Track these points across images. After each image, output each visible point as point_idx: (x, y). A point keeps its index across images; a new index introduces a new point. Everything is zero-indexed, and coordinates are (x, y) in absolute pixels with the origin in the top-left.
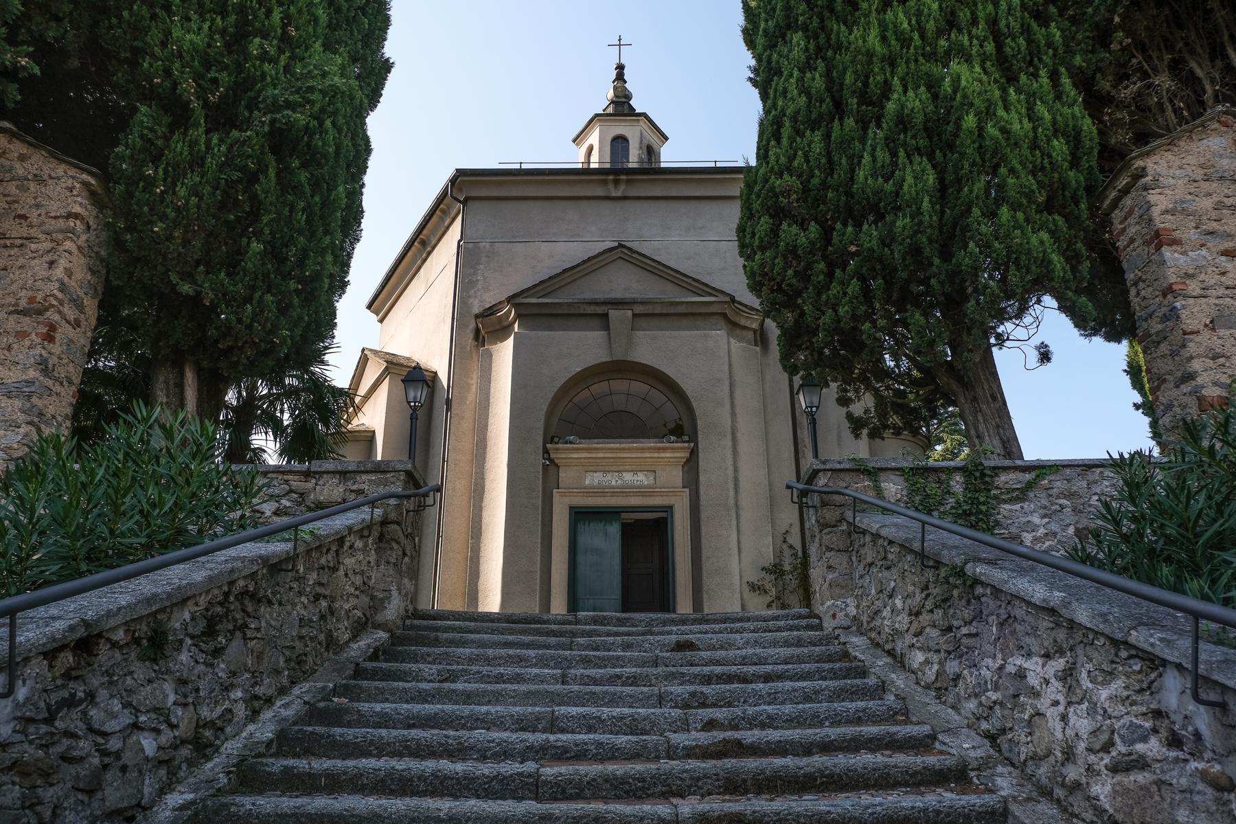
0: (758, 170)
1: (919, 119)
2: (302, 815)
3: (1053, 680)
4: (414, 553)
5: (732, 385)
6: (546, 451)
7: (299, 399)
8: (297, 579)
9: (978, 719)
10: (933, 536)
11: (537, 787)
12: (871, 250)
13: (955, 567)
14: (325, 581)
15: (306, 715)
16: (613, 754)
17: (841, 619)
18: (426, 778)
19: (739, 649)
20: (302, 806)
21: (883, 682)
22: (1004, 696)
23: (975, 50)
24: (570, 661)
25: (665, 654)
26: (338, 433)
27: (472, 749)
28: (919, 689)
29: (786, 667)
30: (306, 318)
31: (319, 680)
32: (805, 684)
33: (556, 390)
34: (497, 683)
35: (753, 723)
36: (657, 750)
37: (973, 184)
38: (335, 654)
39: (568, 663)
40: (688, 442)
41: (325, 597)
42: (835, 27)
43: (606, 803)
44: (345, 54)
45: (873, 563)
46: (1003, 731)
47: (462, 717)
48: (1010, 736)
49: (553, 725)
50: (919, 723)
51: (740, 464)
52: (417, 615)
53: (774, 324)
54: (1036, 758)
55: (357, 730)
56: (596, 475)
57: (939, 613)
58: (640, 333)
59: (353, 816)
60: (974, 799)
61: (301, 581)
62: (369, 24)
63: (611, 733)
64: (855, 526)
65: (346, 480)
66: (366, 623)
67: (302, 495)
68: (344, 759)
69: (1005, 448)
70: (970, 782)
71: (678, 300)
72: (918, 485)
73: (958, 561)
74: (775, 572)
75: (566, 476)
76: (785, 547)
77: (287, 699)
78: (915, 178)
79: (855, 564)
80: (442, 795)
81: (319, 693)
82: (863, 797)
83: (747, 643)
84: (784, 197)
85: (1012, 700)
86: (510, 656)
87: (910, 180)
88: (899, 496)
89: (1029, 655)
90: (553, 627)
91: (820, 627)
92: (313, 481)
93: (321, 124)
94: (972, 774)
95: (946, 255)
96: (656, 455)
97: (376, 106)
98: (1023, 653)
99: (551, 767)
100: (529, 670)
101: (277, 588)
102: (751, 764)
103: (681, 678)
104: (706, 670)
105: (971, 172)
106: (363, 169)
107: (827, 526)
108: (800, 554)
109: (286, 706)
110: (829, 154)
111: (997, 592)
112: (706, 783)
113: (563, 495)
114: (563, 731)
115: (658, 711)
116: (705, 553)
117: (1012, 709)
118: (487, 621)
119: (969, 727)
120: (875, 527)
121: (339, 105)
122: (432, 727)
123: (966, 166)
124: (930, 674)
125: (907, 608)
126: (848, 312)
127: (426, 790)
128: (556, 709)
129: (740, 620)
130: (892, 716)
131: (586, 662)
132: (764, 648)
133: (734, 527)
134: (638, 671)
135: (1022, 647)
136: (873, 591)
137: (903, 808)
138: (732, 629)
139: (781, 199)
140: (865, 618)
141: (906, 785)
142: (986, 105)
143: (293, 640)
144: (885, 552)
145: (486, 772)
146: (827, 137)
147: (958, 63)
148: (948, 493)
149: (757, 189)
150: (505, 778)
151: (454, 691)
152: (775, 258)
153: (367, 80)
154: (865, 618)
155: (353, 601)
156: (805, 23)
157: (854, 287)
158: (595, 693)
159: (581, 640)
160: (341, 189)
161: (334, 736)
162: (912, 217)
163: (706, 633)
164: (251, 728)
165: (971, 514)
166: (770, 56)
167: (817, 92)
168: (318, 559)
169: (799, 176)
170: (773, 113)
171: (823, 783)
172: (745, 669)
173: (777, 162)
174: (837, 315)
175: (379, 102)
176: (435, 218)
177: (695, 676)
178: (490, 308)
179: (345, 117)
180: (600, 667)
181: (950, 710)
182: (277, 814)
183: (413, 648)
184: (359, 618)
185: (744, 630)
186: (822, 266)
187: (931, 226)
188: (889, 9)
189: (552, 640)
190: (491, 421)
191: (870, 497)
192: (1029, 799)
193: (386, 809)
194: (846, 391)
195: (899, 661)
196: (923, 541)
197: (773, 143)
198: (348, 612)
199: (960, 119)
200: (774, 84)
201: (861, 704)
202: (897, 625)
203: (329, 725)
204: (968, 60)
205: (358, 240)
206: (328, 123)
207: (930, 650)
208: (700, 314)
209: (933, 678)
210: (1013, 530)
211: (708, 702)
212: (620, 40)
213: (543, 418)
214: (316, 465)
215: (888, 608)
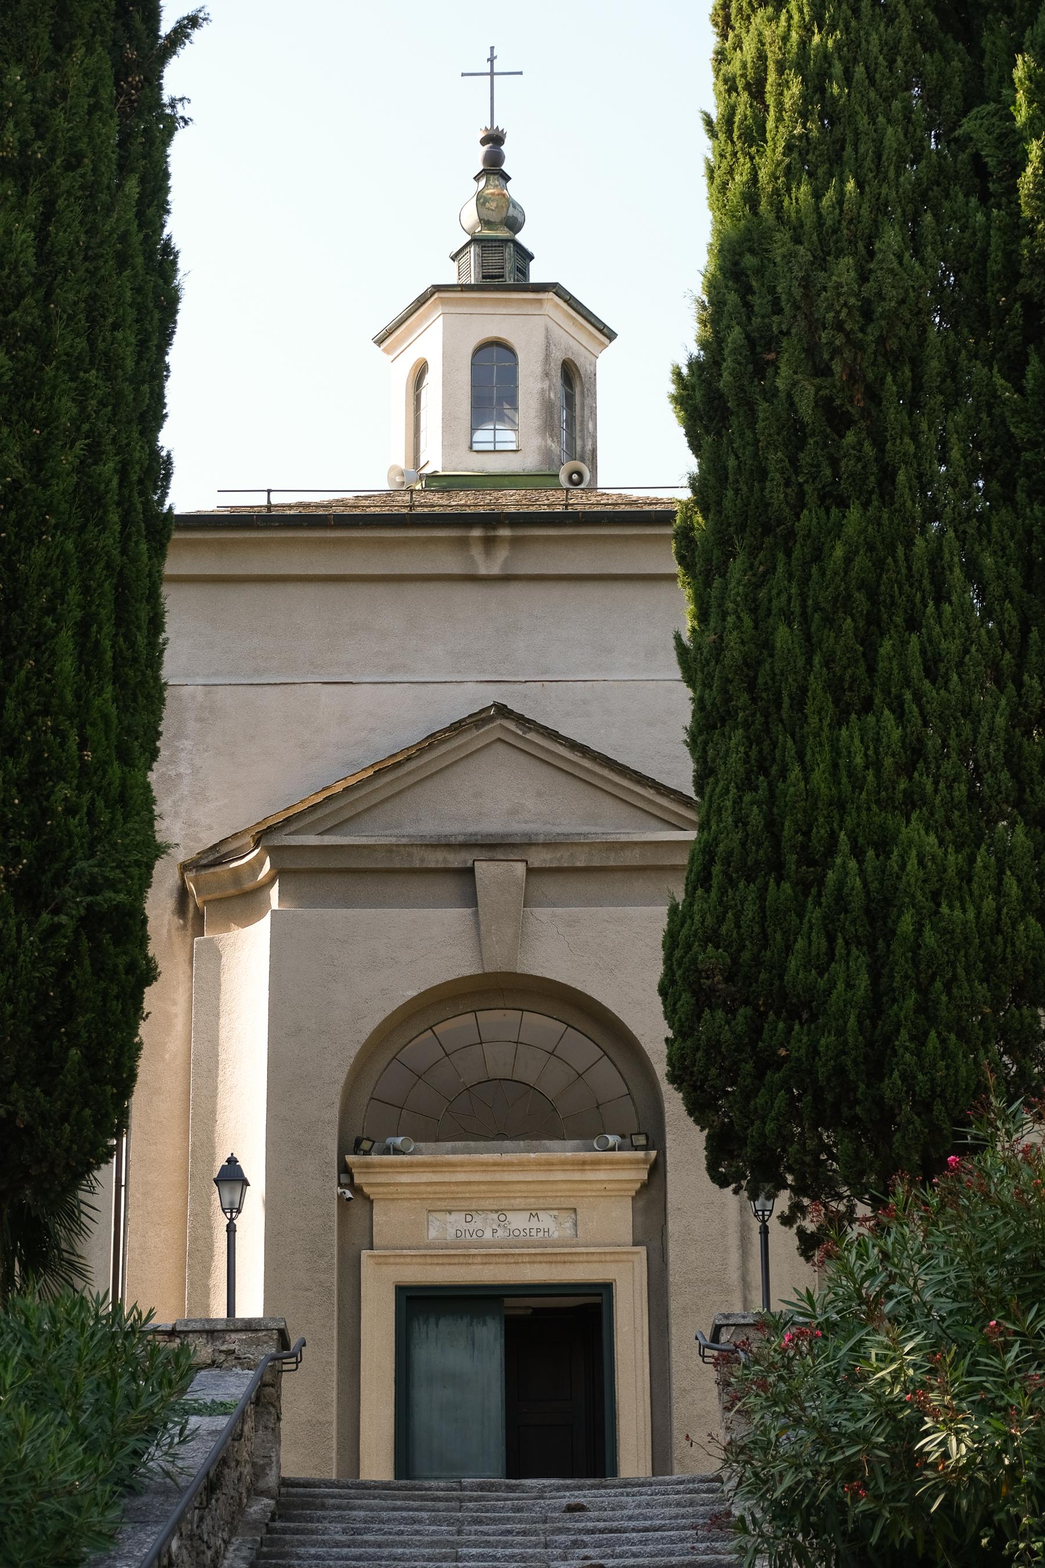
6: (344, 1169)
33: (364, 1037)
40: (645, 1148)
58: (542, 913)
65: (213, 1339)
71: (624, 838)
113: (381, 1261)
115: (543, 1551)
146: (762, 896)
159: (471, 1505)
178: (215, 846)
189: (441, 1505)
212: (491, 60)
213: (337, 1101)
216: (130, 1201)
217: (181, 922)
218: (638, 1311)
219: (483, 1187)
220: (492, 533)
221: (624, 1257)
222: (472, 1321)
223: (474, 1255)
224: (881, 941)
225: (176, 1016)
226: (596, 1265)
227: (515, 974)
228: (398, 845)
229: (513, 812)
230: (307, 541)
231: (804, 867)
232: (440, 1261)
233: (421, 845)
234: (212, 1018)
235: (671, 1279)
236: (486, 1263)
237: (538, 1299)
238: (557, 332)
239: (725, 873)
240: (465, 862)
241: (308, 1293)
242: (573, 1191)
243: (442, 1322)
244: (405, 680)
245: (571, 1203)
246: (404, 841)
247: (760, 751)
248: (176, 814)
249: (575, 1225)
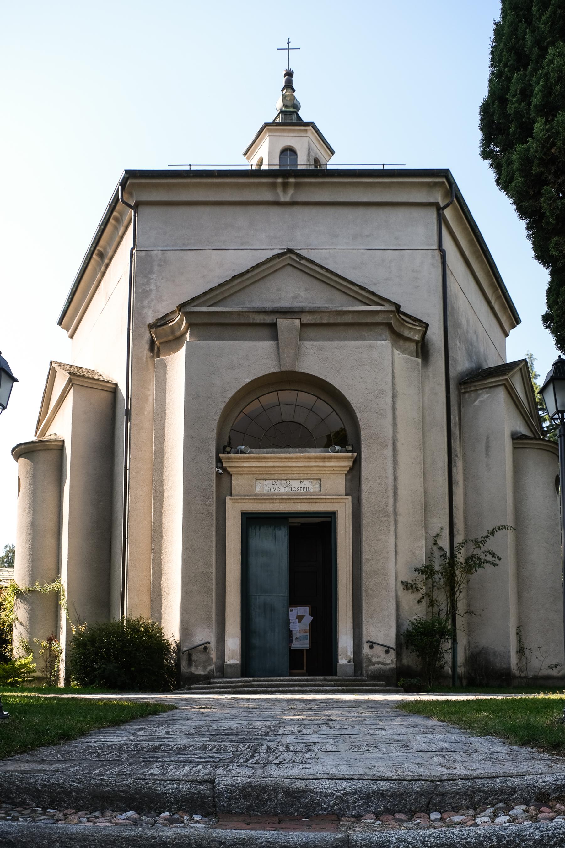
5: (394, 396)
6: (219, 460)
33: (227, 400)
58: (307, 344)
75: (238, 483)
76: (435, 548)
113: (235, 501)
116: (366, 555)
133: (392, 533)
176: (109, 228)
190: (167, 431)
208: (366, 324)
212: (288, 43)
216: (131, 476)
217: (152, 354)
218: (347, 524)
219: (280, 469)
220: (286, 180)
221: (342, 500)
222: (275, 528)
223: (276, 499)
225: (149, 395)
226: (329, 504)
227: (295, 372)
228: (242, 312)
229: (295, 298)
230: (206, 185)
232: (261, 501)
233: (253, 312)
234: (163, 394)
235: (363, 510)
236: (281, 503)
237: (303, 519)
238: (313, 146)
240: (273, 320)
241: (202, 515)
242: (319, 471)
243: (262, 529)
244: (248, 248)
245: (319, 476)
246: (245, 309)
248: (150, 307)
249: (320, 486)
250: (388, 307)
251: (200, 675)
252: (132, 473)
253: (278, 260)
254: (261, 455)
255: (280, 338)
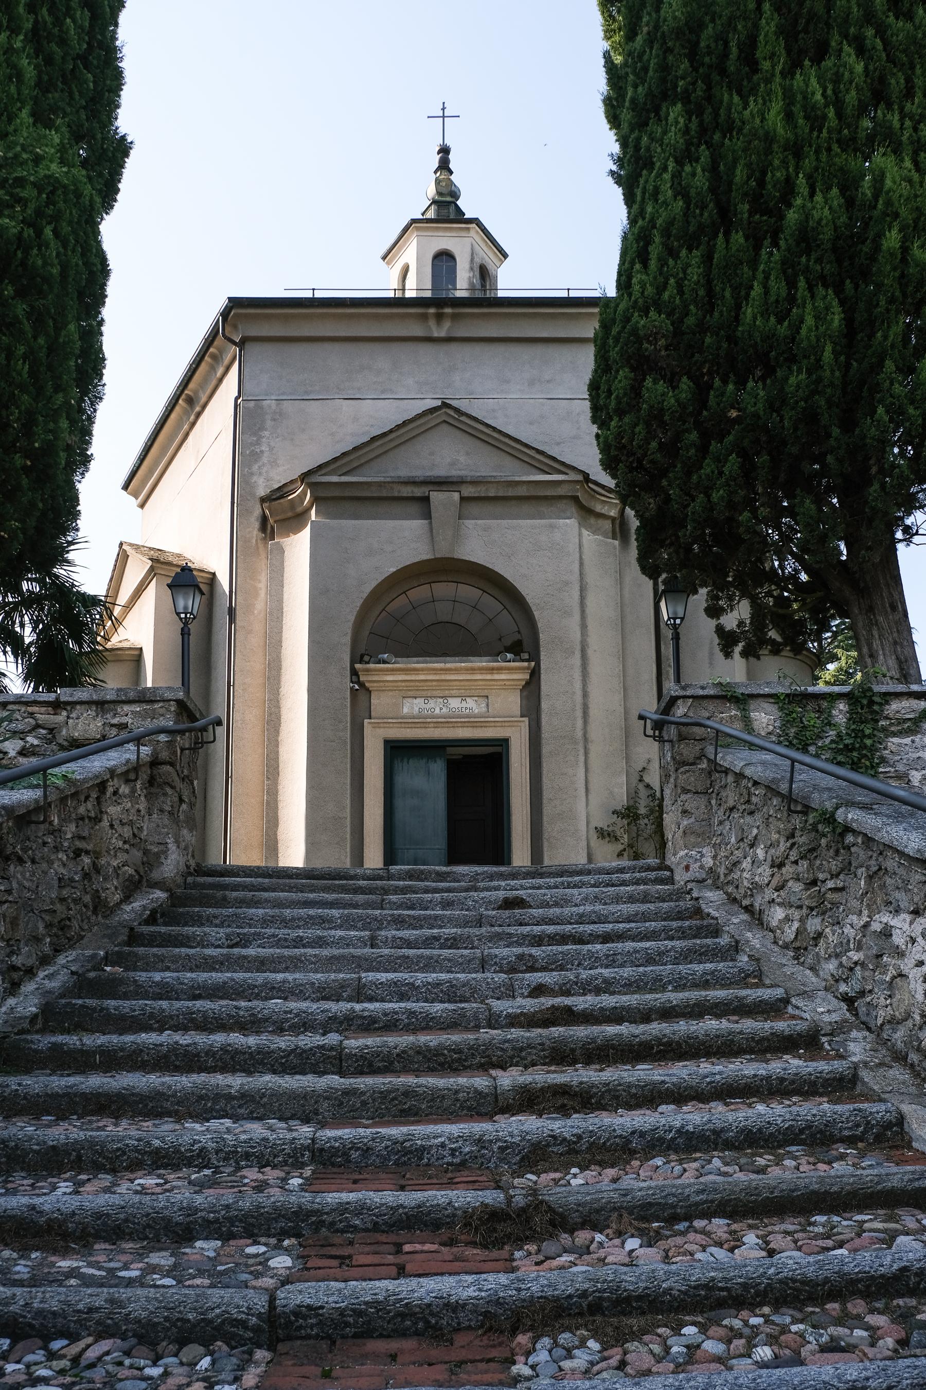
0: (617, 306)
1: (827, 234)
2: (75, 1095)
3: (920, 939)
4: (193, 799)
5: (583, 590)
6: (354, 673)
7: (42, 609)
8: (52, 833)
9: (837, 981)
10: (803, 776)
11: (341, 1061)
12: (756, 415)
13: (824, 813)
14: (85, 833)
15: (74, 986)
16: (428, 1024)
17: (695, 871)
18: (214, 1053)
19: (576, 905)
20: (75, 1085)
21: (737, 942)
22: (866, 956)
23: (906, 134)
24: (381, 922)
25: (490, 913)
26: (94, 651)
27: (266, 1020)
28: (776, 949)
29: (628, 926)
30: (41, 505)
31: (87, 948)
32: (648, 944)
33: (365, 595)
34: (295, 947)
35: (586, 988)
36: (476, 1018)
37: (889, 327)
38: (105, 917)
39: (380, 924)
41: (87, 852)
42: (726, 97)
43: (417, 1076)
44: (64, 129)
45: (734, 807)
46: (862, 993)
47: (256, 986)
48: (868, 999)
49: (360, 993)
50: (772, 986)
51: (590, 688)
52: (201, 871)
53: (633, 513)
54: (893, 1022)
55: (134, 1002)
56: (416, 701)
57: (804, 864)
58: (469, 523)
59: (133, 1094)
60: (823, 1066)
61: (56, 834)
62: (94, 82)
63: (426, 1001)
64: (716, 764)
65: (104, 712)
66: (140, 881)
67: (51, 731)
68: (121, 1034)
69: (901, 669)
70: (821, 1047)
71: (517, 479)
72: (794, 715)
73: (829, 805)
74: (628, 816)
75: (379, 702)
76: (641, 786)
77: (51, 970)
78: (817, 318)
79: (715, 808)
80: (234, 1071)
81: (88, 961)
82: (702, 1065)
83: (586, 899)
84: (650, 343)
85: (874, 961)
86: (311, 917)
87: (809, 320)
88: (771, 728)
89: (897, 911)
90: (362, 883)
91: (671, 880)
92: (64, 713)
93: (39, 233)
94: (824, 1039)
95: (848, 424)
96: (489, 677)
97: (112, 207)
98: (891, 909)
99: (356, 1038)
100: (333, 932)
101: (28, 843)
102: (581, 1032)
103: (509, 940)
104: (537, 929)
105: (888, 310)
106: (99, 299)
107: (685, 763)
108: (658, 794)
109: (50, 977)
110: (709, 282)
111: (868, 840)
112: (530, 1054)
113: (376, 726)
114: (371, 999)
115: (479, 976)
116: (547, 794)
117: (874, 971)
118: (283, 877)
119: (826, 989)
120: (738, 766)
121: (61, 205)
122: (222, 998)
123: (882, 303)
124: (790, 933)
125: (769, 859)
126: (723, 497)
127: (216, 1066)
128: (363, 975)
129: (580, 873)
130: (743, 979)
131: (399, 922)
132: (605, 904)
133: (582, 764)
134: (459, 931)
135: (891, 903)
136: (733, 840)
137: (744, 1076)
138: (569, 883)
139: (645, 345)
140: (722, 871)
141: (751, 1051)
142: (914, 215)
143: (52, 903)
144: (749, 794)
145: (283, 1045)
146: (708, 258)
147: (884, 154)
148: (829, 724)
149: (615, 330)
150: (304, 1051)
151: (245, 957)
152: (636, 425)
153: (97, 168)
154: (722, 871)
155: (122, 857)
156: (686, 91)
157: (733, 463)
158: (408, 957)
159: (393, 898)
160: (72, 327)
161: (107, 1009)
162: (809, 373)
163: (539, 888)
164: (11, 1001)
165: (853, 749)
166: (638, 139)
167: (698, 194)
168: (75, 808)
169: (668, 315)
170: (640, 223)
171: (659, 1052)
172: (581, 928)
173: (643, 293)
174: (709, 500)
175: (115, 200)
176: (203, 367)
177: (524, 937)
178: (280, 488)
179: (70, 223)
180: (415, 928)
181: (808, 972)
182: (47, 1094)
183: (197, 909)
184: (131, 875)
185: (582, 885)
186: (694, 436)
187: (832, 384)
188: (798, 71)
189: (360, 898)
190: (285, 635)
191: (735, 729)
192: (881, 1065)
193: (170, 1087)
194: (718, 598)
195: (757, 918)
196: (791, 781)
197: (638, 266)
198: (116, 869)
199: (880, 235)
200: (642, 181)
201: (709, 966)
202: (757, 879)
203: (102, 997)
204: (897, 151)
205: (101, 399)
206: (48, 232)
207: (791, 906)
208: (546, 498)
209: (793, 937)
210: (901, 767)
211: (537, 965)
212: (443, 109)
213: (349, 632)
214: (65, 694)
215: (749, 859)
224: (848, 281)
229: (453, 464)
230: (334, 316)
231: (757, 216)
239: (664, 244)
245: (485, 693)
246: (388, 480)
247: (701, 124)
250: (573, 476)
251: (206, 1238)
252: (238, 689)
253: (430, 417)
254: (409, 666)
255: (433, 515)
